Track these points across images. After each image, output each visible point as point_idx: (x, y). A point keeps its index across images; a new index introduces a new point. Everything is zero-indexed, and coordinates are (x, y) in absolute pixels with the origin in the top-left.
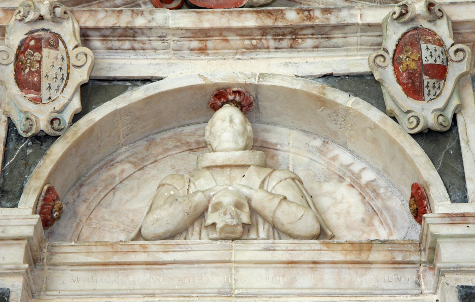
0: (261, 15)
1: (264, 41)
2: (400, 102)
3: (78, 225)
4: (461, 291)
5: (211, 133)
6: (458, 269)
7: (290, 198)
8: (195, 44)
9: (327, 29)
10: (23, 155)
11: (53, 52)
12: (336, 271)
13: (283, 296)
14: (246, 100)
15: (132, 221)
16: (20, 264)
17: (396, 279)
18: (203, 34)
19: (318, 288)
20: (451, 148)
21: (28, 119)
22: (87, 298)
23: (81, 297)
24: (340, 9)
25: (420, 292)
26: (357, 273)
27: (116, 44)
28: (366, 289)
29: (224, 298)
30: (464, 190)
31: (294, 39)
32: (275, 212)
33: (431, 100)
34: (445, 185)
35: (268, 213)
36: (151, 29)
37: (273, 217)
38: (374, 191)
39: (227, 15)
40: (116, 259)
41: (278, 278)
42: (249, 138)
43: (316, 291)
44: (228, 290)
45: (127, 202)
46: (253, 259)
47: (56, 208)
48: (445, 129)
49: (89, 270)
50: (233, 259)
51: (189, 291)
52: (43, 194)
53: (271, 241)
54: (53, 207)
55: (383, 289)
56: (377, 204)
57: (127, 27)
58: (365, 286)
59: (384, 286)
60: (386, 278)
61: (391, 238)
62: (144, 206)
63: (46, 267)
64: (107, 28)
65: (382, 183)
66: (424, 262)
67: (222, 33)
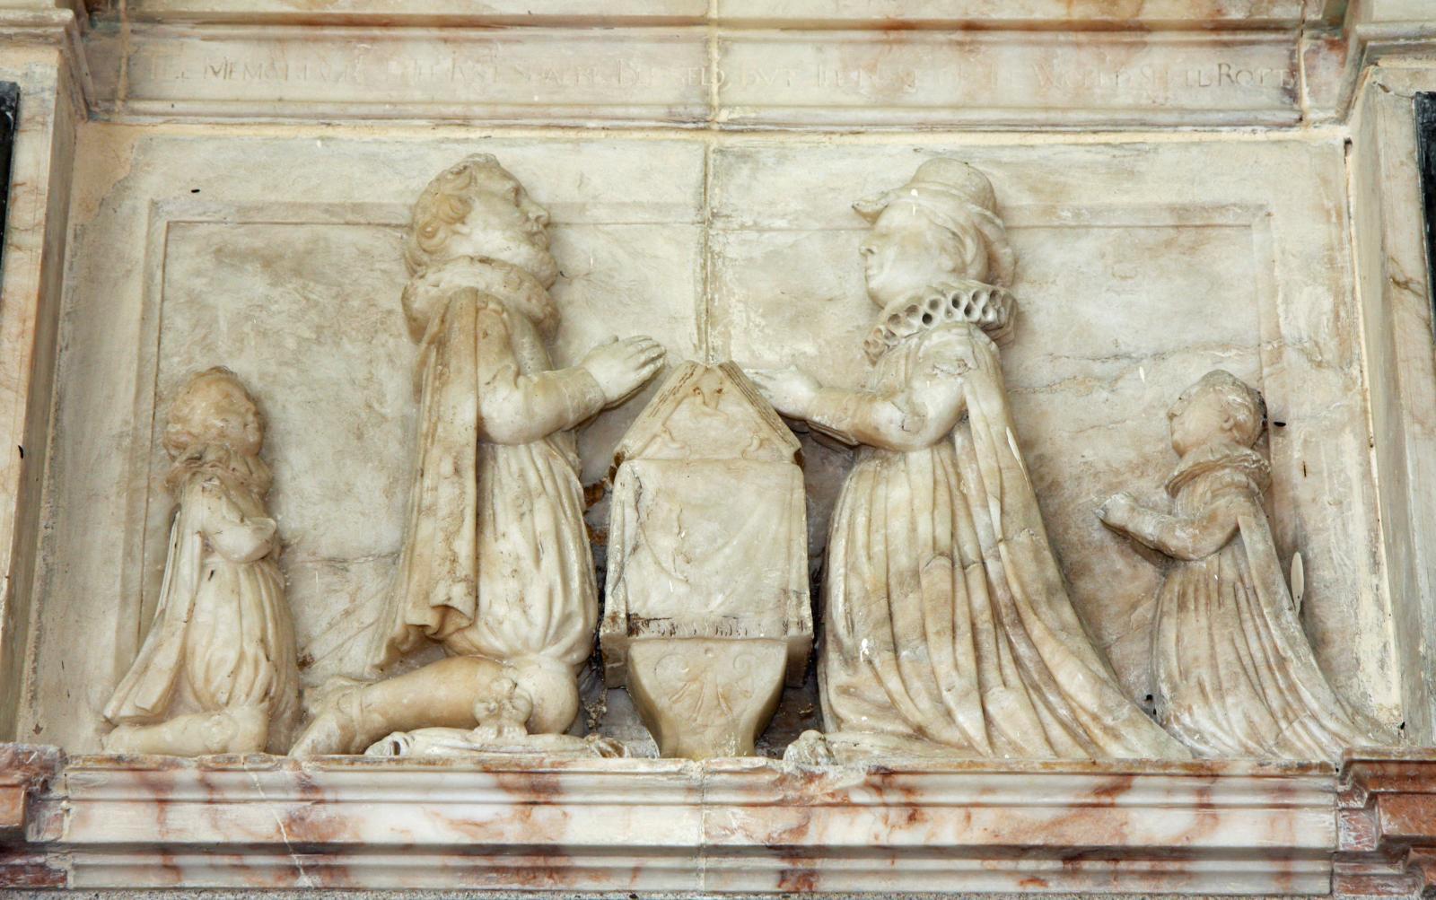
4: (1425, 110)
6: (1423, 41)
12: (1037, 52)
13: (869, 128)
16: (47, 8)
17: (1225, 79)
19: (980, 107)
22: (260, 124)
23: (241, 120)
25: (1296, 116)
26: (1103, 60)
28: (1128, 109)
29: (684, 135)
41: (854, 75)
44: (698, 111)
49: (260, 39)
50: (714, 14)
51: (577, 111)
55: (1182, 110)
58: (1124, 99)
59: (1186, 100)
60: (1193, 75)
63: (126, 27)
66: (1314, 25)
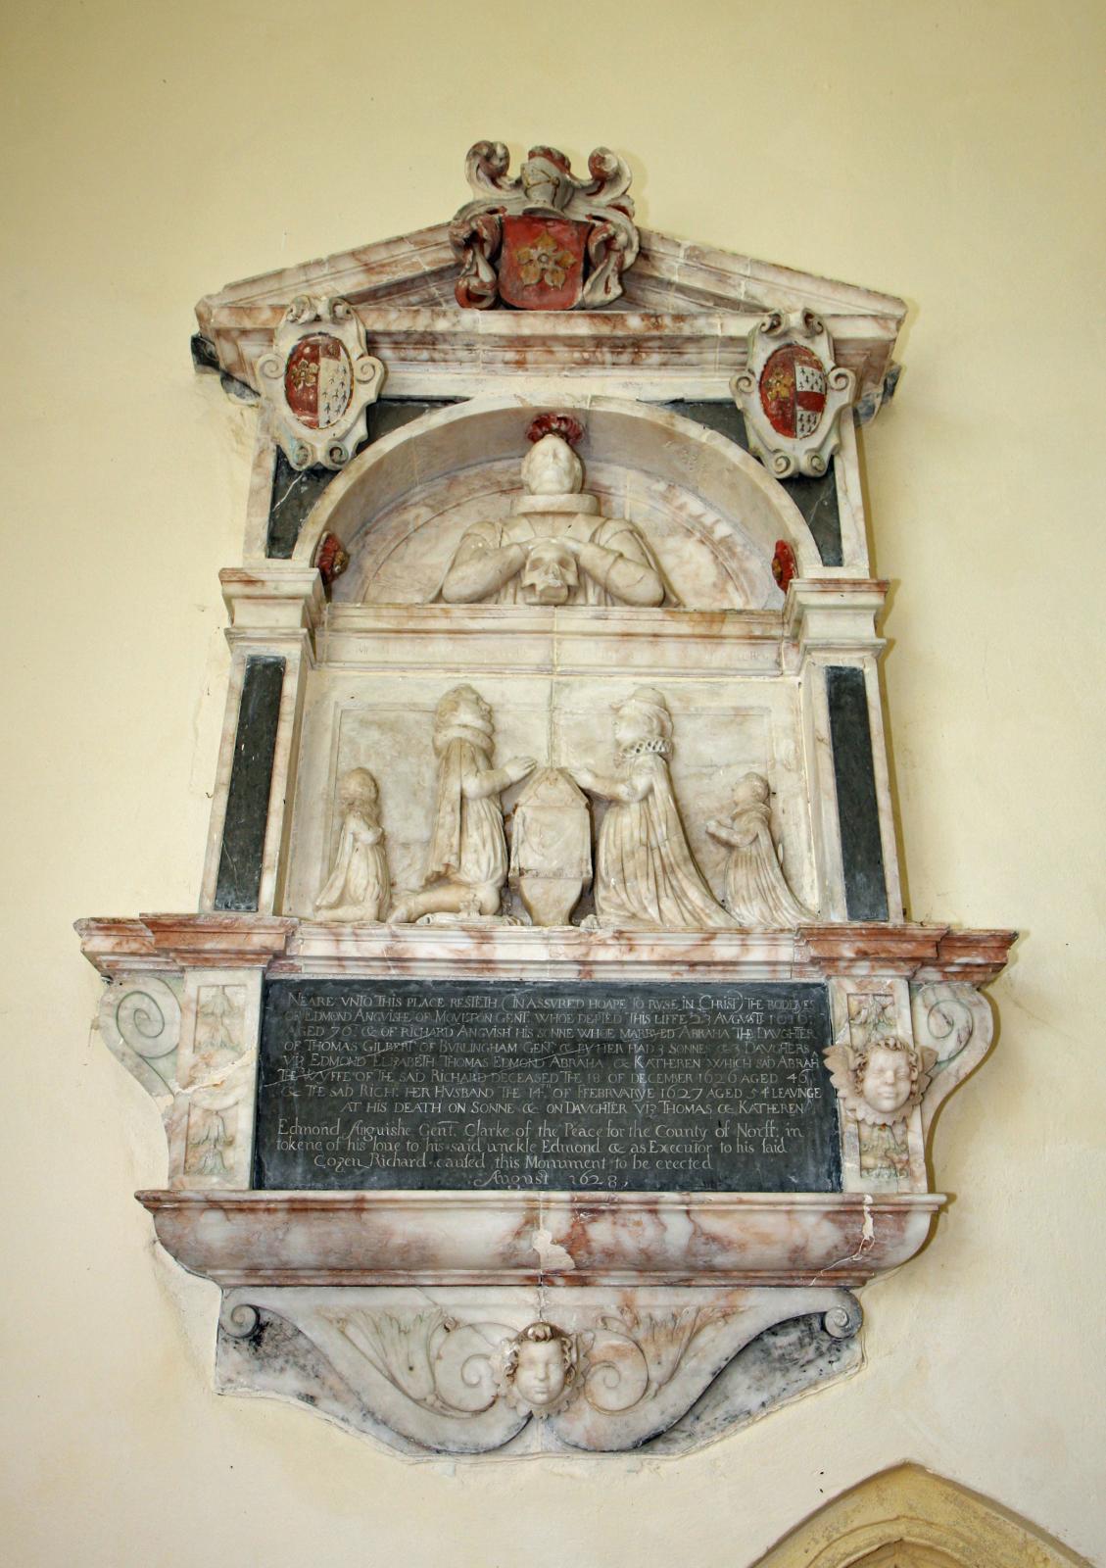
0: (596, 321)
1: (598, 355)
2: (766, 438)
3: (363, 583)
5: (528, 471)
7: (627, 554)
8: (511, 356)
9: (678, 341)
10: (296, 495)
11: (333, 362)
14: (572, 429)
15: (430, 579)
18: (521, 343)
20: (826, 499)
21: (302, 448)
24: (694, 316)
27: (411, 353)
30: (838, 550)
31: (636, 353)
32: (608, 572)
33: (805, 437)
34: (817, 544)
35: (599, 572)
36: (455, 334)
37: (606, 579)
38: (729, 549)
39: (552, 318)
40: (411, 625)
42: (576, 478)
43: (656, 670)
44: (549, 667)
45: (423, 555)
46: (580, 629)
47: (337, 560)
48: (819, 475)
49: (379, 638)
50: (555, 629)
52: (322, 543)
53: (603, 608)
54: (334, 560)
55: (737, 669)
56: (732, 565)
57: (425, 332)
59: (738, 666)
61: (748, 608)
62: (445, 560)
64: (399, 333)
65: (738, 539)
67: (546, 342)
